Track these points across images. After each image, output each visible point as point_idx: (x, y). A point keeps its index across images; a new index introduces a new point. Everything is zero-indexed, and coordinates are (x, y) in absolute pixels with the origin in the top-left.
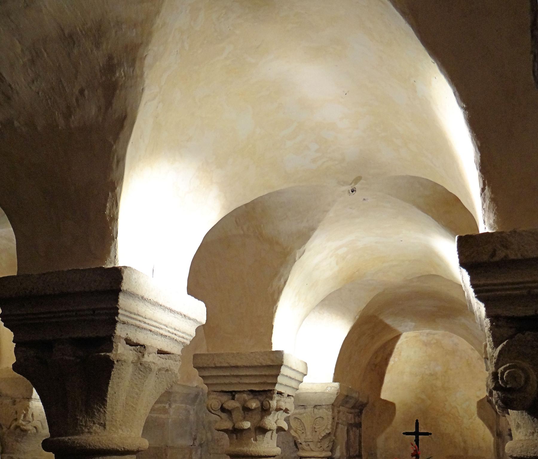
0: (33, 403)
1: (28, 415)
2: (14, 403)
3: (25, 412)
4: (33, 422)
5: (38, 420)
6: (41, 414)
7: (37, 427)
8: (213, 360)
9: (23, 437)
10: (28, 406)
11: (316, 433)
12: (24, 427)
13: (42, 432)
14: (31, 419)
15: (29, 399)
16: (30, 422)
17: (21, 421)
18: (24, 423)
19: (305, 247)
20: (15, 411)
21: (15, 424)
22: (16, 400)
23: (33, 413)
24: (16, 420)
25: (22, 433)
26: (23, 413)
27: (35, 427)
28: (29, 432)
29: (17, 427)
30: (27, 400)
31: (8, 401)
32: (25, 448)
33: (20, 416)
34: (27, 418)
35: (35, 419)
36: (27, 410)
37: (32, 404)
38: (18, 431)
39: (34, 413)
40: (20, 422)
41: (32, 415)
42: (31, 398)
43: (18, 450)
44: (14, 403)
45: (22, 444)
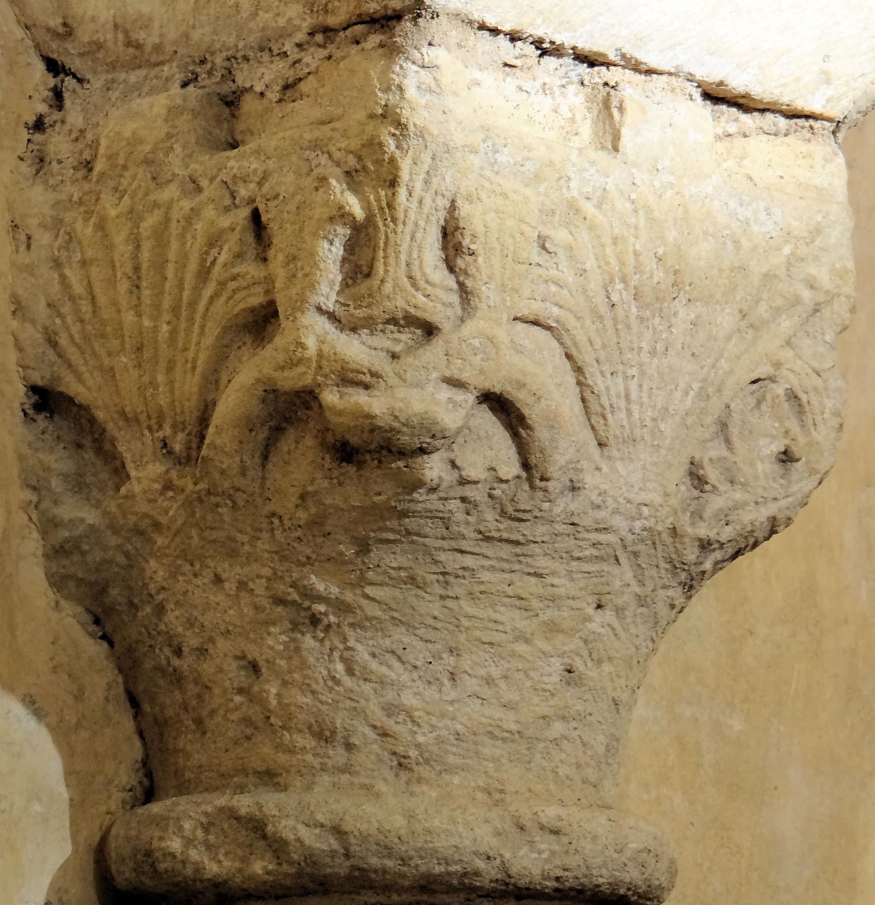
0: (446, 78)
1: (404, 234)
3: (355, 206)
4: (468, 329)
6: (560, 236)
8: (758, 400)
9: (364, 548)
12: (359, 398)
13: (590, 479)
16: (430, 330)
19: (553, 471)
20: (245, 213)
26: (342, 215)
30: (375, 39)
31: (159, 103)
32: (408, 700)
37: (434, 90)
39: (464, 209)
40: (311, 343)
45: (362, 654)
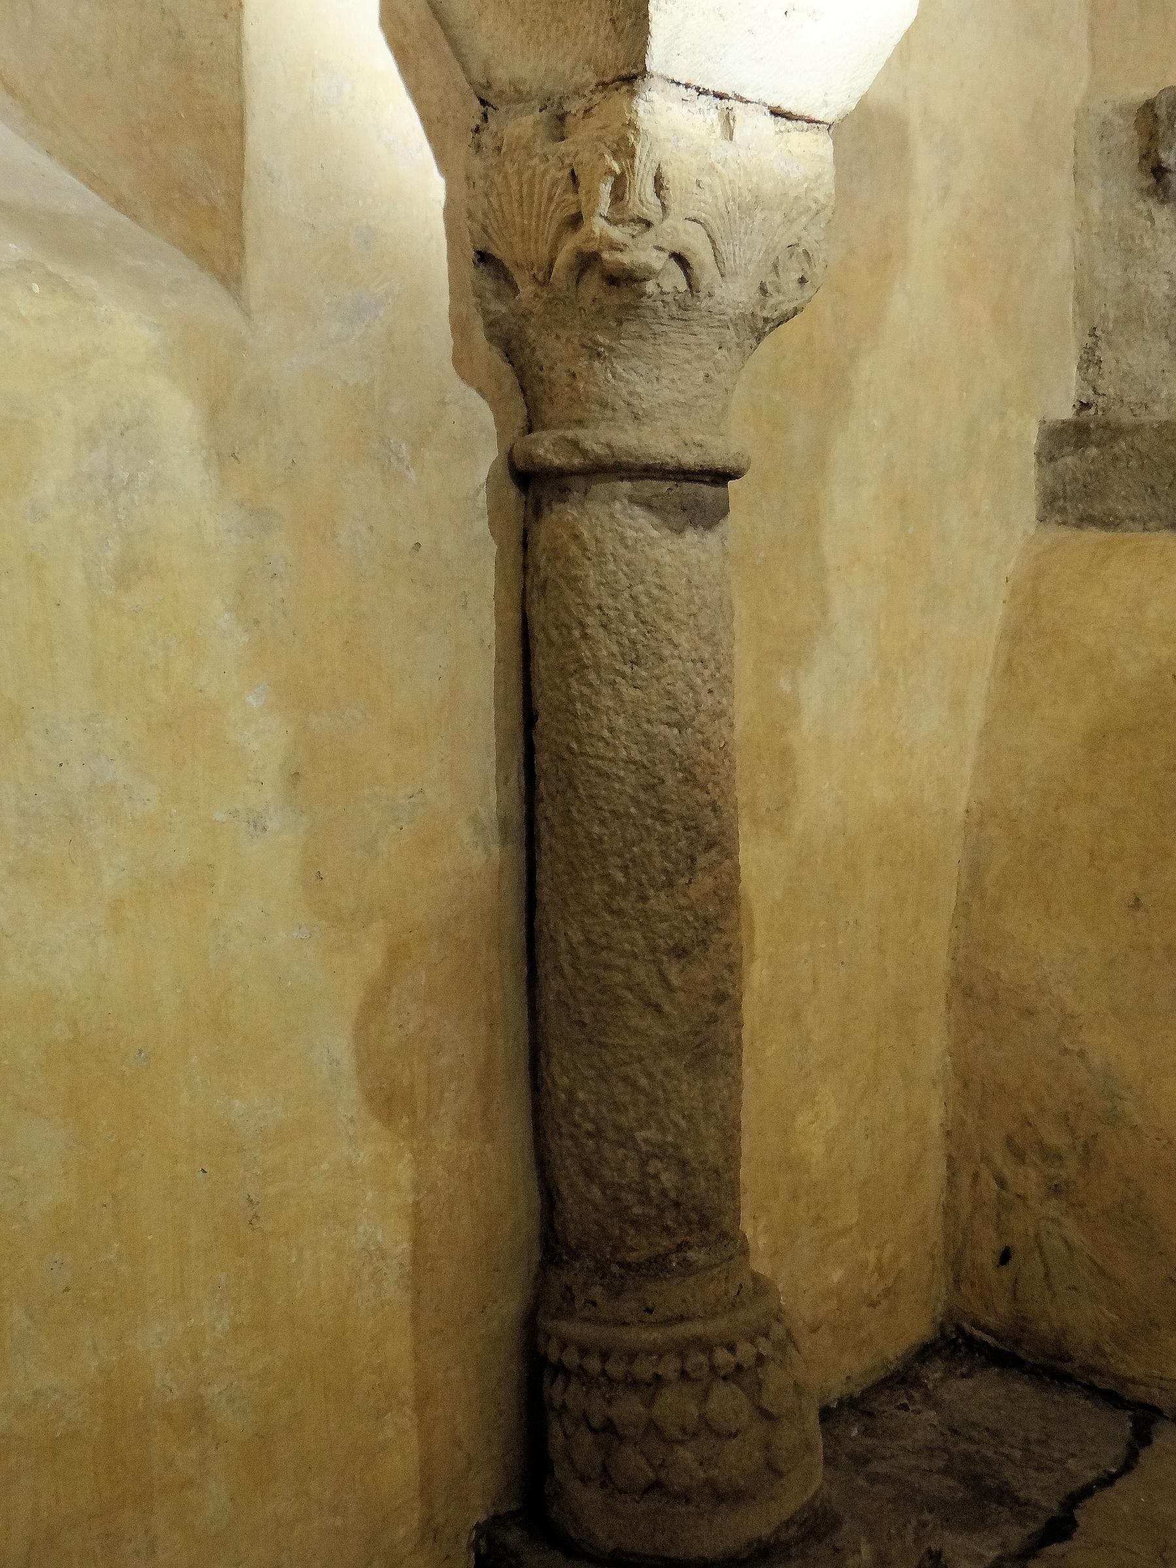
0: (657, 107)
2: (559, 127)
5: (693, 214)
7: (688, 255)
9: (620, 322)
10: (631, 125)
11: (712, 695)
12: (619, 256)
14: (650, 206)
15: (630, 79)
16: (649, 224)
17: (598, 226)
18: (617, 234)
20: (567, 171)
21: (571, 244)
22: (566, 107)
23: (659, 167)
24: (576, 221)
25: (614, 299)
26: (610, 171)
27: (680, 259)
28: (650, 287)
29: (587, 261)
30: (625, 88)
33: (593, 194)
34: (632, 198)
35: (674, 207)
36: (625, 151)
38: (592, 286)
39: (664, 168)
40: (597, 231)
41: (659, 183)
42: (644, 73)
43: (604, 405)
44: (559, 127)
